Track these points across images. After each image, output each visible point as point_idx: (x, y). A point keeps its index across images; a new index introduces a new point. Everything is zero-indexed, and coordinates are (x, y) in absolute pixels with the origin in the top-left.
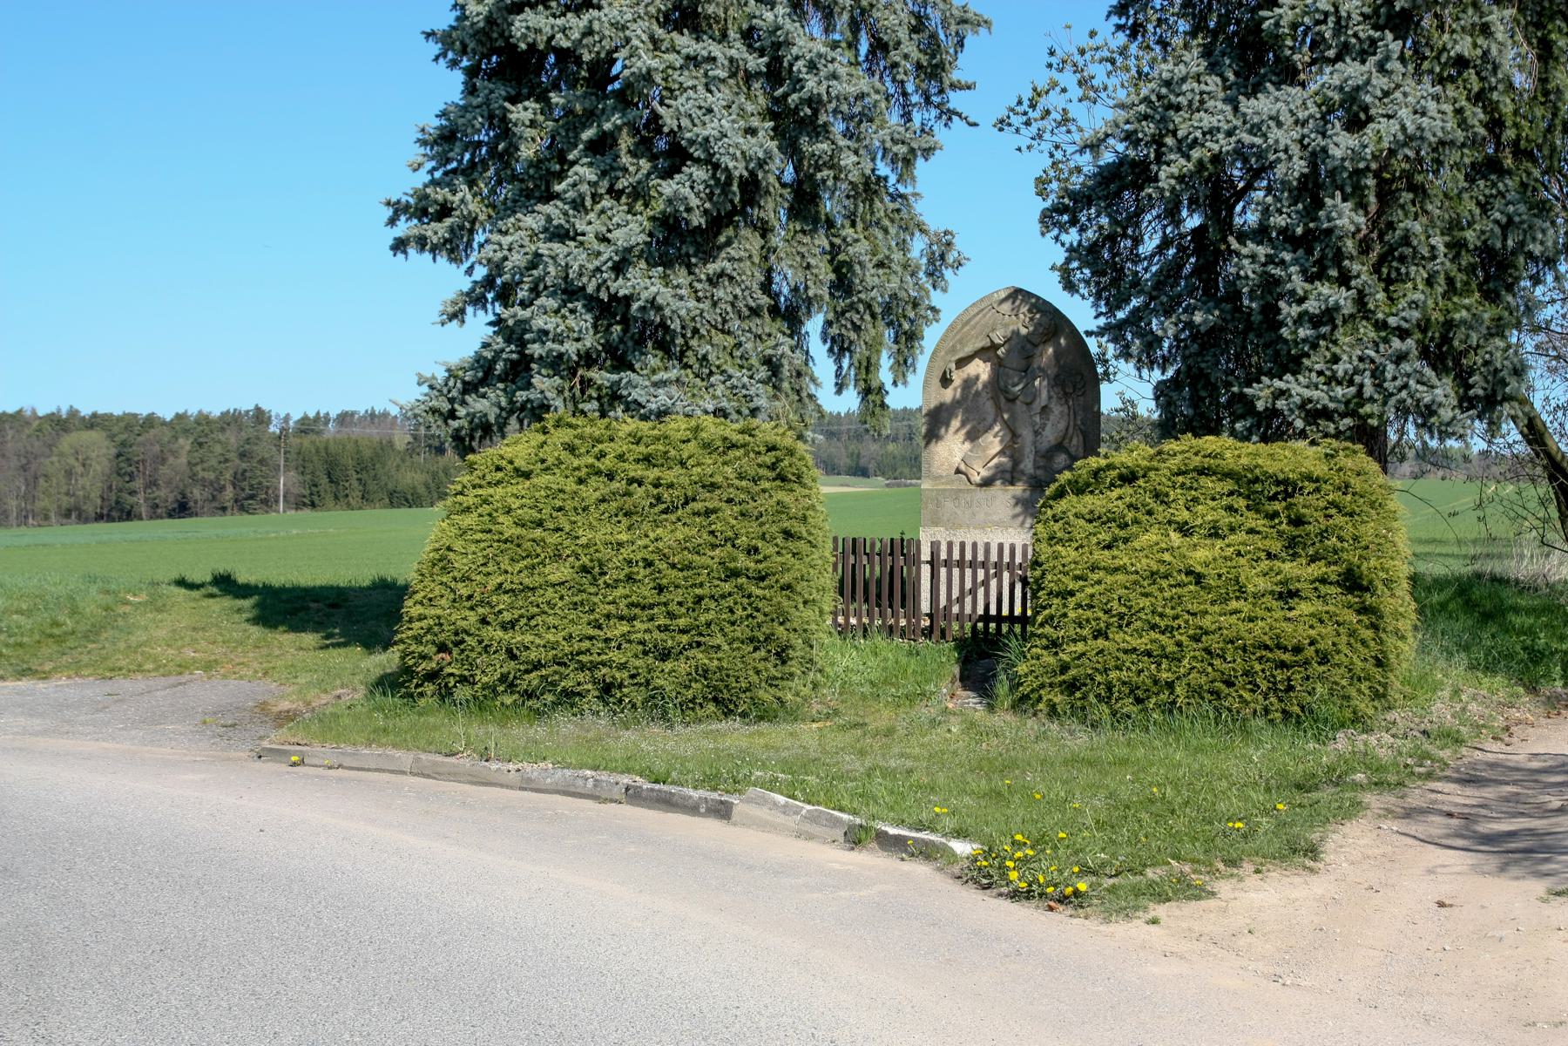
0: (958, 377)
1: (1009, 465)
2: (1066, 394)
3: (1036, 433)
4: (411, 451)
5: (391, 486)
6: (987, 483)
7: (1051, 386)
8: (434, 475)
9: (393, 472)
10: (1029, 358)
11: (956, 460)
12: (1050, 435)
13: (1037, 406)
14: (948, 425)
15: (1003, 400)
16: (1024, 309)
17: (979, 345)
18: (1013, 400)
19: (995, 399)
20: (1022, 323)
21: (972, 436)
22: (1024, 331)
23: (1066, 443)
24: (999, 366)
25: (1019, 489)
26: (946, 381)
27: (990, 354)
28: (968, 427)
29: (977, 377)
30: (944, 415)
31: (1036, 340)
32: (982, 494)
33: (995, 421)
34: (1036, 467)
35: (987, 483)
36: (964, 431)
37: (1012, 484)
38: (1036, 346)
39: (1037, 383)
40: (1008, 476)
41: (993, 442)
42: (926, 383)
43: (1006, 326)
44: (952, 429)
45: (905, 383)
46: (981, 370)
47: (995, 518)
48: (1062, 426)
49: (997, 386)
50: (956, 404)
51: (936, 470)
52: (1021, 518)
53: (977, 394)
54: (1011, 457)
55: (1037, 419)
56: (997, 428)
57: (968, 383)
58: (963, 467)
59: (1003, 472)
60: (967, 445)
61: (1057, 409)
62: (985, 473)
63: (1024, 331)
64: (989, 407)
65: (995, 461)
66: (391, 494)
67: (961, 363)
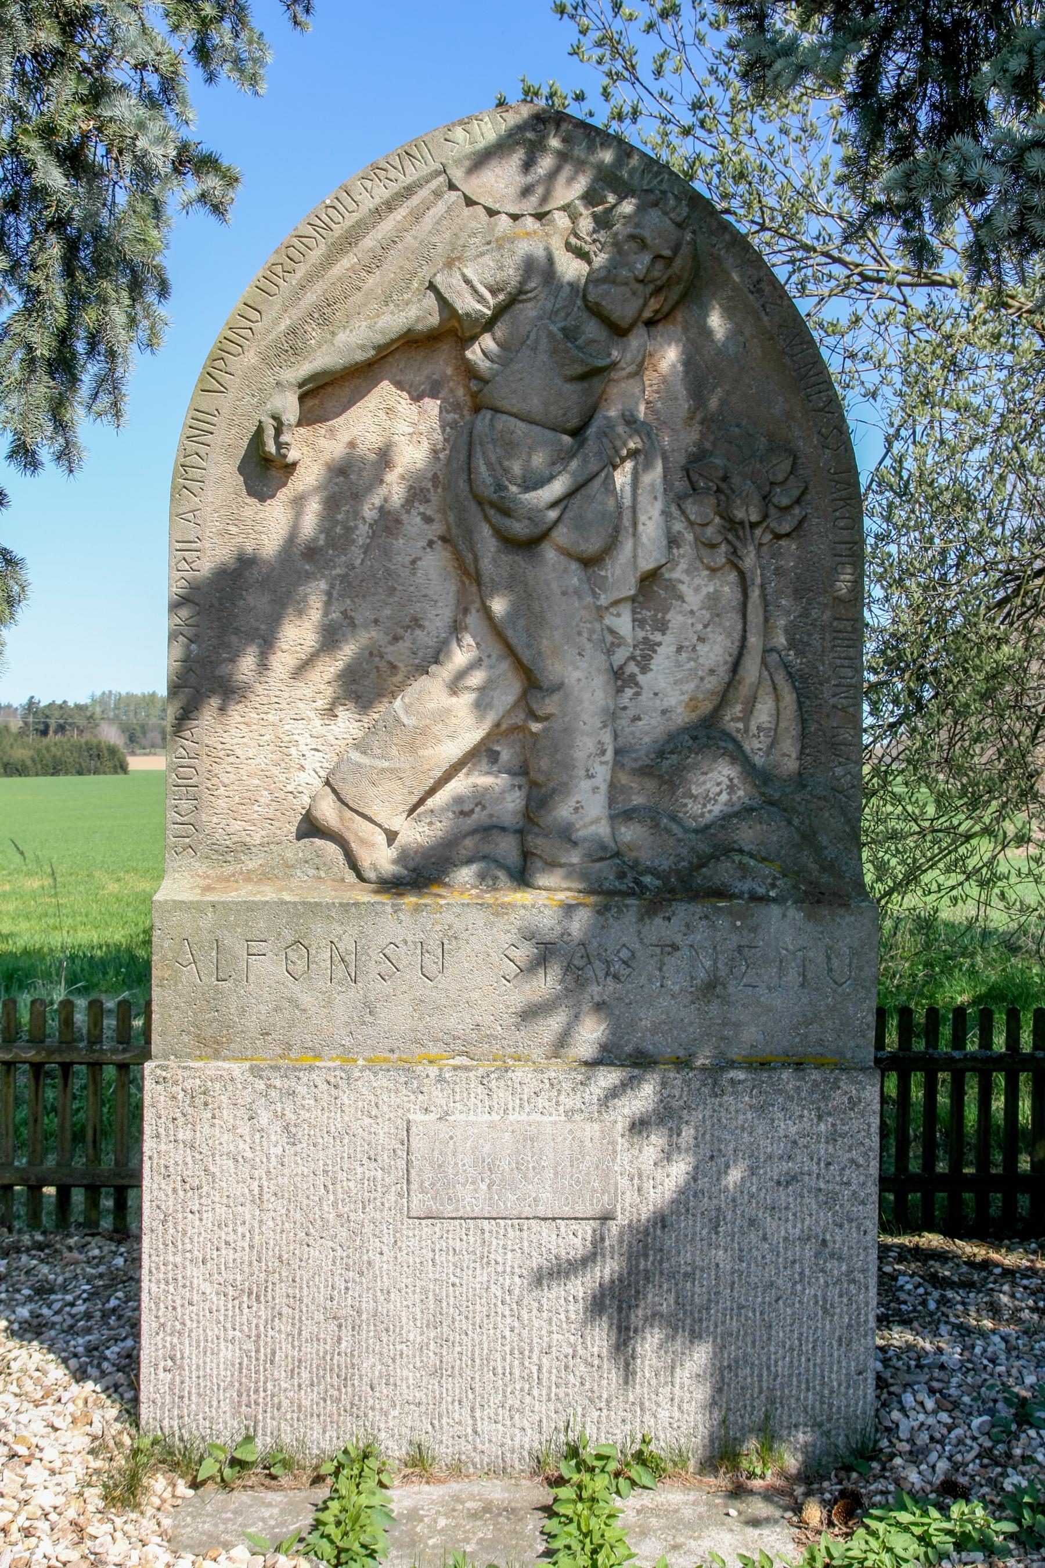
0: (312, 453)
1: (513, 803)
2: (732, 525)
3: (620, 678)
4: (22, 733)
5: (5, 760)
6: (419, 875)
7: (679, 496)
8: (39, 751)
9: (8, 749)
10: (594, 375)
11: (306, 783)
12: (671, 690)
13: (621, 574)
14: (267, 644)
15: (487, 543)
16: (570, 190)
17: (394, 321)
18: (528, 545)
19: (456, 543)
20: (564, 235)
21: (364, 687)
22: (571, 269)
23: (731, 720)
24: (475, 403)
25: (548, 901)
26: (264, 469)
27: (442, 365)
28: (348, 651)
29: (385, 457)
30: (258, 602)
31: (623, 306)
32: (400, 922)
33: (456, 628)
34: (621, 814)
35: (419, 875)
36: (330, 668)
37: (522, 878)
38: (619, 331)
39: (622, 477)
40: (507, 847)
41: (448, 713)
42: (186, 478)
43: (500, 244)
44: (283, 661)
45: (66, 455)
46: (401, 429)
47: (456, 1022)
48: (715, 652)
49: (468, 496)
50: (303, 559)
51: (220, 818)
52: (555, 1023)
53: (388, 522)
54: (522, 770)
55: (623, 623)
56: (460, 657)
57: (348, 480)
58: (328, 812)
59: (488, 830)
60: (347, 724)
61: (697, 588)
62: (417, 834)
63: (571, 269)
64: (433, 573)
65: (459, 785)
66: (6, 765)
67: (326, 393)
